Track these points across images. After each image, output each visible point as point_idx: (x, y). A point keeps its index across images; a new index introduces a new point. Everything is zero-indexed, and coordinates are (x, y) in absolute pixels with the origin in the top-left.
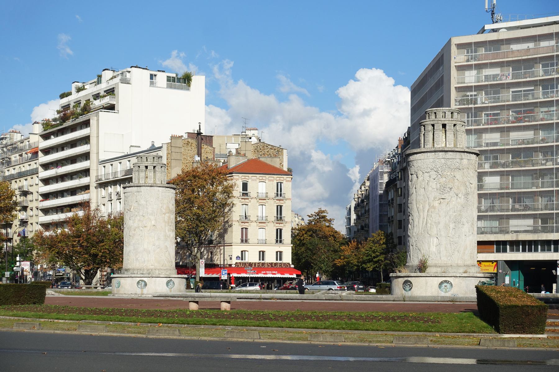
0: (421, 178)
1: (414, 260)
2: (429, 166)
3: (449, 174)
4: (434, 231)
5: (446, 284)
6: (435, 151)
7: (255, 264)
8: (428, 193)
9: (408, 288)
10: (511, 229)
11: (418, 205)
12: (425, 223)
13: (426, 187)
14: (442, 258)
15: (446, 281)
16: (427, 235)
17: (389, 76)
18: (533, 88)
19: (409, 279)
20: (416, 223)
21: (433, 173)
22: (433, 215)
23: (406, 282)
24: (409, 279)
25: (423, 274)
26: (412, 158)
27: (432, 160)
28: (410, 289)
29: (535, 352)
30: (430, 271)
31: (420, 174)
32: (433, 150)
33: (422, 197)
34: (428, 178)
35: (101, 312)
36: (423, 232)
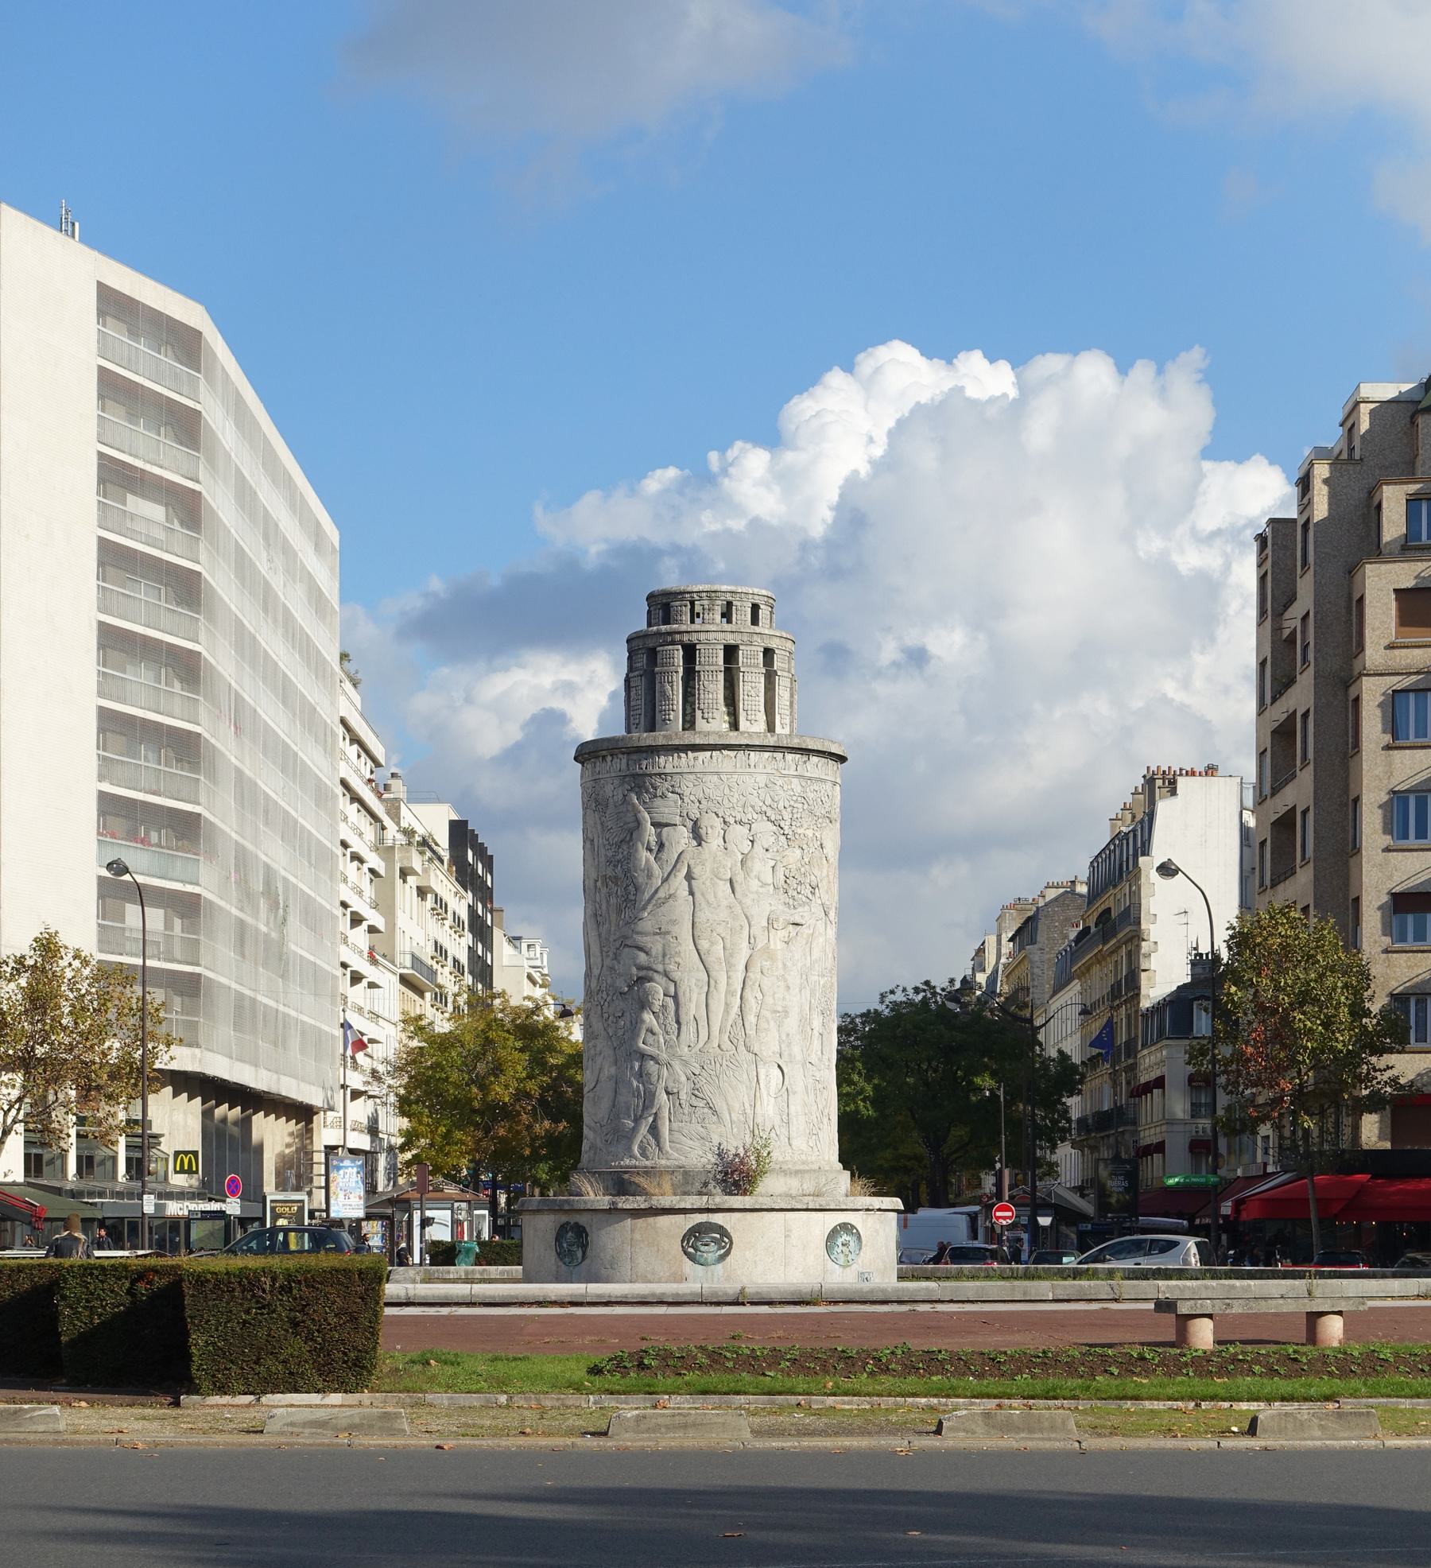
0: (714, 842)
1: (689, 1146)
2: (754, 800)
3: (810, 833)
4: (769, 1043)
5: (845, 1237)
6: (775, 748)
7: (27, 1143)
8: (748, 902)
9: (711, 1252)
10: (762, 1072)
11: (704, 944)
12: (736, 1009)
13: (739, 878)
14: (794, 1143)
15: (846, 1227)
16: (744, 1056)
17: (930, 357)
18: (679, 654)
19: (718, 1219)
20: (693, 1006)
21: (763, 828)
22: (766, 983)
23: (695, 1235)
24: (718, 1219)
25: (736, 1201)
26: (666, 763)
27: (762, 780)
28: (722, 1258)
29: (520, 1455)
30: (770, 1187)
31: (712, 828)
32: (771, 741)
33: (723, 914)
34: (746, 846)
35: (751, 1363)
36: (727, 1045)
